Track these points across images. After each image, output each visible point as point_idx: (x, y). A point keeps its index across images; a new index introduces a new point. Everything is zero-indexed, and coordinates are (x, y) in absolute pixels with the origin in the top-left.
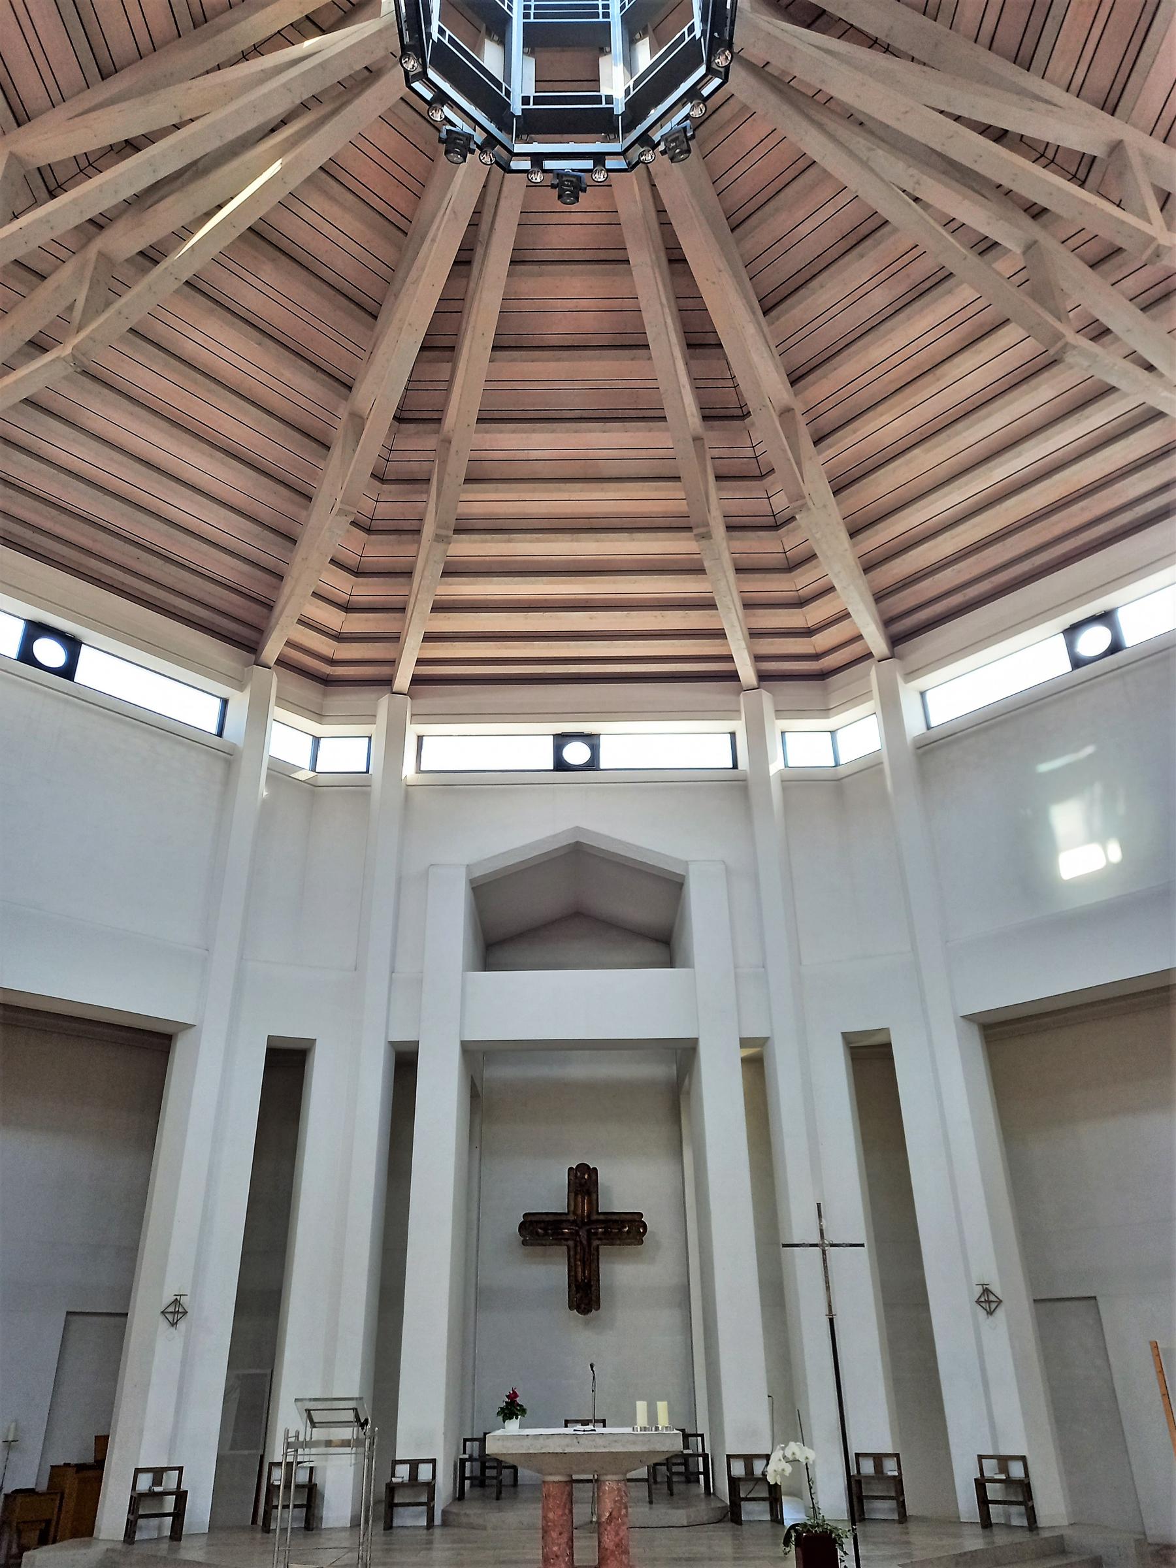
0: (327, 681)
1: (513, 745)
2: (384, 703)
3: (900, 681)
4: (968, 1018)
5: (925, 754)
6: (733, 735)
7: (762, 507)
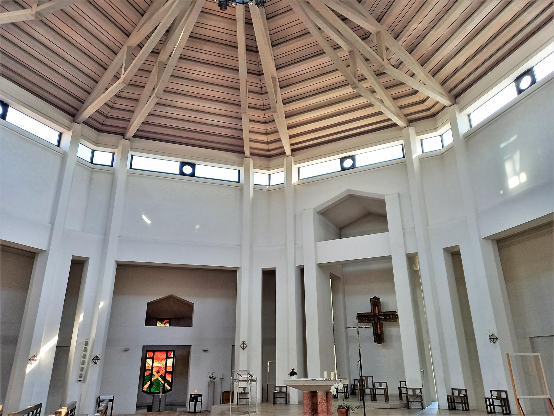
0: (269, 157)
1: (329, 165)
2: (285, 160)
3: (457, 113)
4: (486, 238)
5: (468, 140)
6: (239, 171)
7: (261, 103)
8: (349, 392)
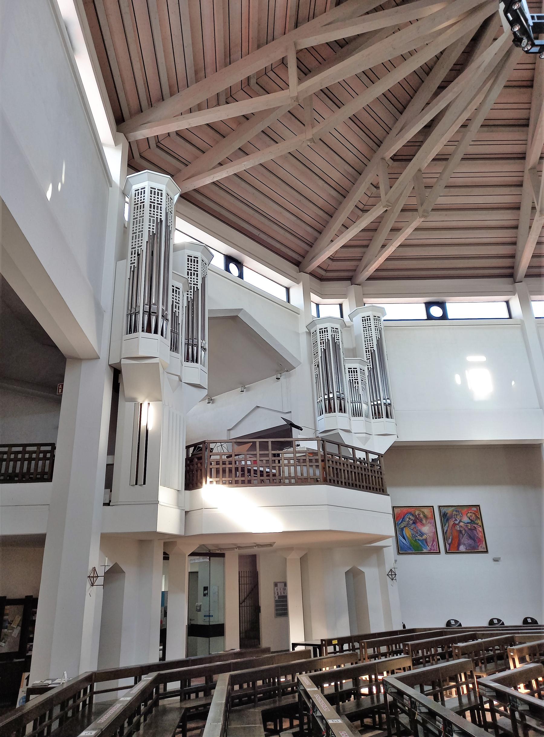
8: (324, 707)
